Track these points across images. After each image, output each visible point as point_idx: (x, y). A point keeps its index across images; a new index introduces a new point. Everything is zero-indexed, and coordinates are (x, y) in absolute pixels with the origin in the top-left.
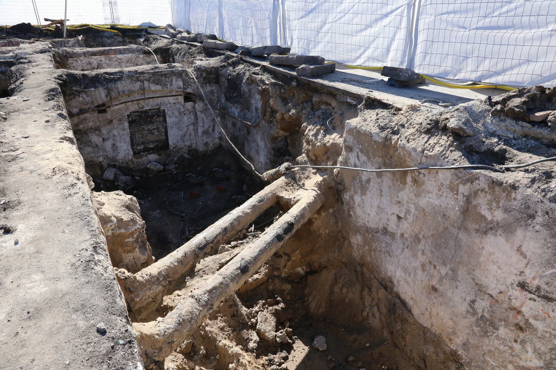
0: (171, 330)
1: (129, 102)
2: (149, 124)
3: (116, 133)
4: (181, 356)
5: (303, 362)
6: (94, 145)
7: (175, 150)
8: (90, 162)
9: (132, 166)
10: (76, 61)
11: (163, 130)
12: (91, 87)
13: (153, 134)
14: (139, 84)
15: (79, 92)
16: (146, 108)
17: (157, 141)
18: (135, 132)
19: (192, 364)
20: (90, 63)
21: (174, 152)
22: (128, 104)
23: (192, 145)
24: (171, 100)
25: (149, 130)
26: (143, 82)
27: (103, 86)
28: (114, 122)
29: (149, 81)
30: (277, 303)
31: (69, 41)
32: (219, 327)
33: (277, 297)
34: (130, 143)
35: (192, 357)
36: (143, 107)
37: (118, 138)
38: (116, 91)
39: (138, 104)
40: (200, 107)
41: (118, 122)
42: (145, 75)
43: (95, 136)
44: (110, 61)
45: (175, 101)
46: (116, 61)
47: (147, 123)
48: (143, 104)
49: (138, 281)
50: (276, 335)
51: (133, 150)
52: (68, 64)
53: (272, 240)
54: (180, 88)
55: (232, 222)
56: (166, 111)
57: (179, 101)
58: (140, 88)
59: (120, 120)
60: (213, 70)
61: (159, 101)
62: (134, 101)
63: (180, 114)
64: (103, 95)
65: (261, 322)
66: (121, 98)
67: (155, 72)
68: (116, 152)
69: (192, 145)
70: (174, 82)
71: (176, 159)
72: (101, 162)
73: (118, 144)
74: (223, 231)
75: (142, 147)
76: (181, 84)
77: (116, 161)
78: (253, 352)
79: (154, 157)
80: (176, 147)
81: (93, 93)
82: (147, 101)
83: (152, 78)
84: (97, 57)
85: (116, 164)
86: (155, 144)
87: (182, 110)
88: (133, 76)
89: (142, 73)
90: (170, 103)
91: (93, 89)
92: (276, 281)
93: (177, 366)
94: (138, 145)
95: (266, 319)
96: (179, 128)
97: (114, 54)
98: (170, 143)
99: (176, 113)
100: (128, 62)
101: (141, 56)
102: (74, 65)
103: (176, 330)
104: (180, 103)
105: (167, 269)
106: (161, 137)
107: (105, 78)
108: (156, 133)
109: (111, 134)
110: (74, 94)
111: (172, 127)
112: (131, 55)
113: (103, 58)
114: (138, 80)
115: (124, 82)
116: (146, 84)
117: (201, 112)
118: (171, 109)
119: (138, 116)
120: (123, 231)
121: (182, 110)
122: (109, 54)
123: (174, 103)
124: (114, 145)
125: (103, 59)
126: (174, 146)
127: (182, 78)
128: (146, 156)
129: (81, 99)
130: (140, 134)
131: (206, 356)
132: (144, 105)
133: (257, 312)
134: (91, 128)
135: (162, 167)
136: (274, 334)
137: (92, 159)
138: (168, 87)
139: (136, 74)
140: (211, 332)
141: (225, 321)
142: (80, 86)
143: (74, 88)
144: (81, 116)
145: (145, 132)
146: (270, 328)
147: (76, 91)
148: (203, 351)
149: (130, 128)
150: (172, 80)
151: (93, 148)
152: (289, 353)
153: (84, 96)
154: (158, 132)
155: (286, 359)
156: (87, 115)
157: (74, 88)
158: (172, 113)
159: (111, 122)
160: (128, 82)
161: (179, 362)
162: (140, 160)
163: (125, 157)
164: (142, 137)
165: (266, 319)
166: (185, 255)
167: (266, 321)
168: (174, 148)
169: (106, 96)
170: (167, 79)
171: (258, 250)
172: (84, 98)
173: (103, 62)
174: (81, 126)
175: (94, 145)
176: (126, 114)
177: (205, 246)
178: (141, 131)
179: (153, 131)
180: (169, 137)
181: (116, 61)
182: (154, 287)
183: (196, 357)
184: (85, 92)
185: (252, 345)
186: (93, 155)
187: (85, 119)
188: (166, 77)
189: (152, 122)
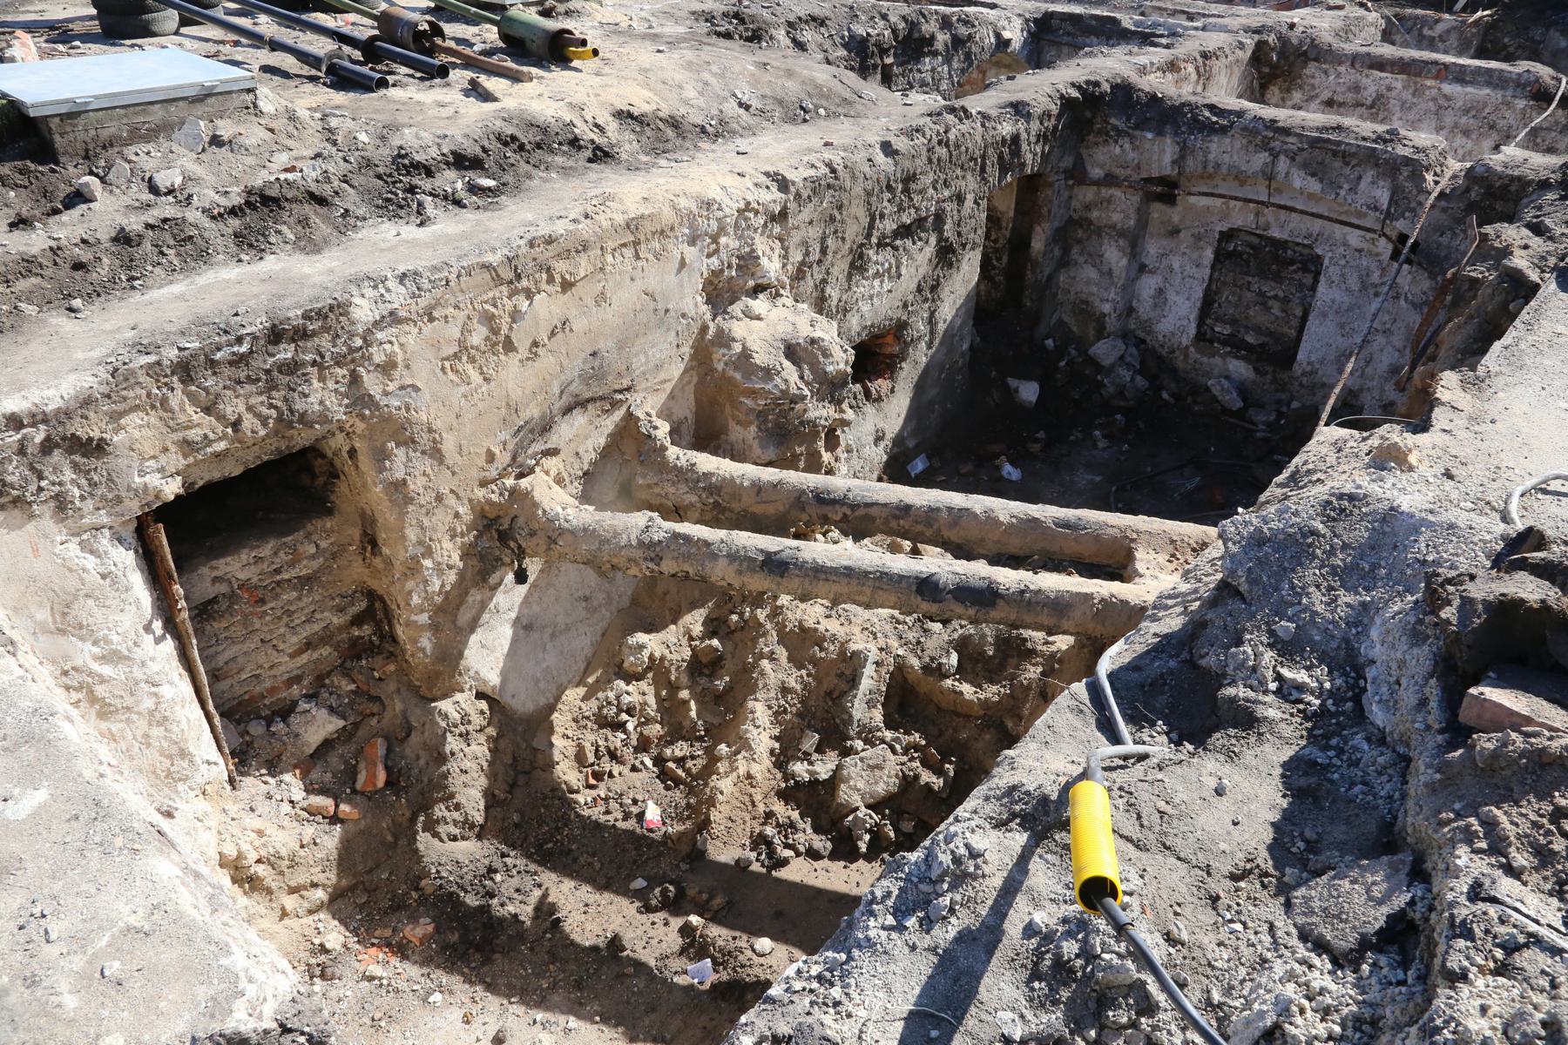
0: (566, 525)
1: (1236, 198)
2: (1267, 278)
3: (1176, 266)
4: (687, 653)
5: (819, 892)
6: (1105, 269)
7: (1305, 380)
8: (1083, 302)
9: (1180, 364)
10: (1326, 72)
11: (1299, 312)
12: (1149, 130)
13: (1268, 309)
14: (1263, 157)
15: (1120, 133)
16: (1275, 233)
17: (1270, 334)
18: (1224, 283)
19: (684, 679)
20: (1356, 88)
21: (1301, 385)
22: (1232, 203)
23: (1361, 390)
24: (1355, 238)
25: (1261, 294)
26: (1275, 156)
27: (1176, 134)
28: (1182, 235)
29: (1293, 159)
30: (939, 772)
31: (1437, 21)
32: (783, 682)
33: (950, 763)
34: (1198, 305)
35: (701, 674)
36: (1267, 228)
37: (1177, 280)
38: (1200, 157)
39: (1257, 215)
40: (1416, 290)
41: (1192, 240)
42: (1291, 139)
43: (1114, 249)
44: (1414, 95)
45: (1364, 245)
46: (1434, 99)
47: (1263, 274)
48: (1271, 219)
49: (664, 457)
50: (857, 809)
51: (1199, 326)
52: (1300, 77)
53: (901, 577)
54: (1376, 209)
55: (938, 509)
56: (1326, 262)
57: (1375, 250)
58: (1263, 172)
59: (1198, 238)
60: (1513, 188)
61: (1317, 225)
62: (1250, 201)
63: (1364, 287)
64: (1168, 158)
65: (862, 760)
66: (1220, 182)
67: (1319, 140)
68: (1158, 311)
69: (1361, 390)
70: (1363, 185)
71: (1295, 405)
72: (1104, 315)
73: (1172, 296)
74: (898, 508)
75: (1227, 330)
76: (1383, 196)
77: (1149, 333)
78: (786, 781)
79: (1243, 371)
80: (1311, 373)
81: (1147, 146)
82: (1283, 214)
83: (1305, 154)
84: (1383, 75)
85: (1148, 339)
86: (1262, 339)
87: (1375, 277)
88: (1258, 133)
89: (1286, 131)
90: (1345, 244)
91: (1149, 135)
92: (988, 737)
93: (663, 658)
94: (1218, 320)
95: (879, 767)
96: (1342, 326)
97: (1436, 78)
98: (1300, 356)
99: (1353, 282)
100: (1466, 111)
101: (1521, 104)
102: (1316, 82)
103: (572, 532)
104: (1377, 255)
105: (724, 479)
106: (1286, 329)
107: (1195, 119)
108: (1276, 311)
109: (1165, 262)
110: (1107, 134)
111: (1325, 315)
112: (1487, 91)
113: (1398, 81)
114: (1265, 146)
115: (1228, 140)
116: (1283, 164)
117: (1413, 304)
118: (1343, 262)
119: (1252, 247)
120: (738, 376)
121: (1375, 277)
122: (1419, 75)
123: (1360, 251)
124: (1160, 291)
125: (1399, 85)
126: (1309, 368)
127: (1394, 178)
128: (1223, 356)
129: (1118, 150)
130: (1233, 294)
131: (719, 698)
132: (1273, 223)
133: (883, 741)
134: (1114, 227)
135: (1240, 404)
136: (857, 801)
137: (1091, 299)
138: (1343, 193)
139: (1267, 128)
140: (762, 674)
141: (805, 686)
142: (1128, 119)
143: (1113, 121)
144: (1103, 190)
145: (1249, 295)
146: (861, 785)
147: (1115, 128)
148: (720, 684)
149: (1213, 267)
150: (1360, 178)
151: (1102, 273)
152: (833, 856)
153: (1127, 146)
154: (1284, 311)
155: (813, 854)
156: (1116, 193)
157: (1113, 121)
158: (1343, 275)
159: (1175, 232)
160: (1238, 144)
161: (675, 657)
162: (1205, 359)
163: (1173, 334)
164: (1236, 306)
165: (879, 767)
166: (776, 486)
167: (872, 768)
168: (1304, 374)
169: (1174, 162)
170: (1347, 171)
171: (846, 563)
172: (1123, 151)
173: (1394, 93)
174: (1095, 214)
175: (1105, 269)
176: (1219, 228)
177: (834, 502)
178: (1240, 287)
179: (1270, 303)
180: (1305, 338)
181: (1434, 99)
182: (683, 488)
183: (703, 681)
184: (1131, 137)
185: (799, 769)
186: (1095, 289)
187: (1109, 201)
188: (1347, 164)
189: (1278, 278)
